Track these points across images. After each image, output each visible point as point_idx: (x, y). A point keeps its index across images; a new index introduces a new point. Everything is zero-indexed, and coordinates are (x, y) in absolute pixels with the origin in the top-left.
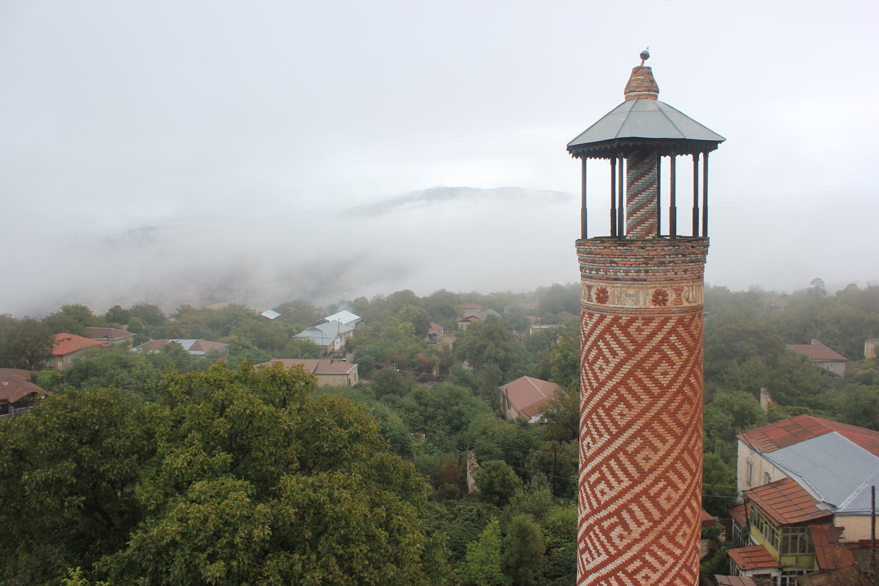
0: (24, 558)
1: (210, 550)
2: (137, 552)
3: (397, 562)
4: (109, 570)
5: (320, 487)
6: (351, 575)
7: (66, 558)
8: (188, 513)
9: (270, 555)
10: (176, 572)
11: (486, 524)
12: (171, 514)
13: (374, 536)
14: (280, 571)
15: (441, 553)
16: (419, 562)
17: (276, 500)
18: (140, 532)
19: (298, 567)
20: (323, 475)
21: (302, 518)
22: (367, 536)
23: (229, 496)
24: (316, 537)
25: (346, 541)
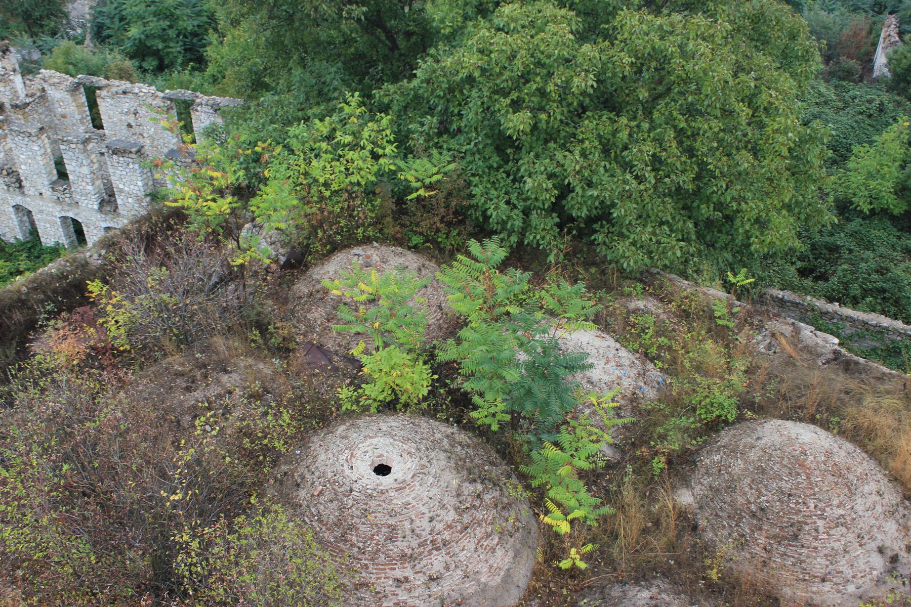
0: (297, 72)
1: (514, 95)
2: (425, 85)
3: (755, 152)
4: (391, 101)
5: (671, 33)
6: (691, 157)
7: (343, 80)
8: (491, 44)
9: (589, 113)
10: (470, 116)
11: (887, 124)
12: (470, 43)
13: (732, 112)
14: (599, 137)
15: (817, 151)
16: (785, 158)
17: (607, 43)
18: (430, 60)
19: (624, 135)
20: (677, 17)
21: (640, 71)
22: (723, 110)
23: (547, 28)
24: (654, 100)
25: (691, 112)
